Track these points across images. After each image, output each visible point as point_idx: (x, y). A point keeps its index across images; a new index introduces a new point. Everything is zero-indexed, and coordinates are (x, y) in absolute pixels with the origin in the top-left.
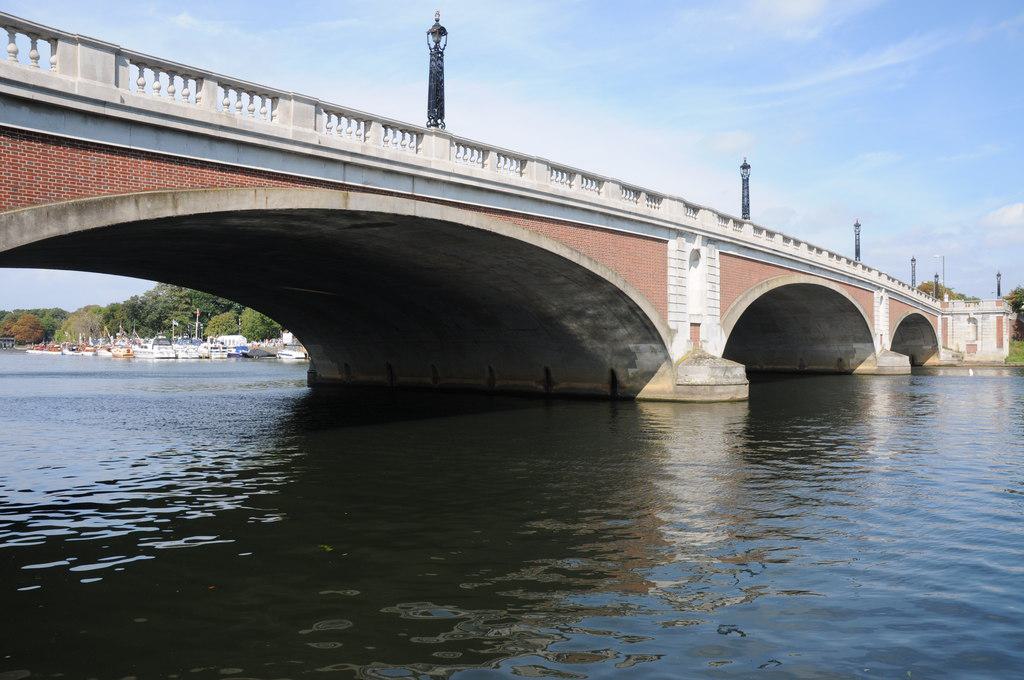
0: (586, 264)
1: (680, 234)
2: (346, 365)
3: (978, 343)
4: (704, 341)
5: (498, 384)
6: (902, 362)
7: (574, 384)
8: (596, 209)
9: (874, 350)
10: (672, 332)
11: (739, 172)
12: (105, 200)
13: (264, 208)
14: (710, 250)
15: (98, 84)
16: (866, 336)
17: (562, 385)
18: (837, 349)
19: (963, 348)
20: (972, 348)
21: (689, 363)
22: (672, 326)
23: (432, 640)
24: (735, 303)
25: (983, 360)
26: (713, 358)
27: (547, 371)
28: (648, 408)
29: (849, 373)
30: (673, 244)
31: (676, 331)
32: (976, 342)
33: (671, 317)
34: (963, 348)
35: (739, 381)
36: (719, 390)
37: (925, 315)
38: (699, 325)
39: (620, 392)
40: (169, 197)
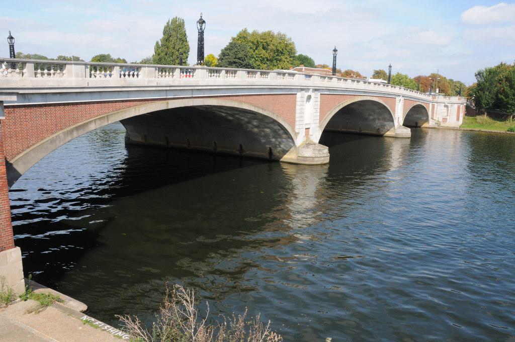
0: (261, 111)
1: (302, 90)
2: (145, 136)
3: (448, 117)
4: (311, 135)
5: (219, 150)
6: (407, 132)
7: (253, 153)
8: (266, 87)
9: (394, 125)
10: (297, 134)
11: (332, 52)
12: (85, 124)
13: (138, 114)
14: (316, 94)
15: (80, 79)
16: (391, 120)
17: (247, 153)
18: (377, 124)
19: (441, 120)
20: (445, 120)
21: (304, 147)
22: (297, 131)
23: (98, 196)
24: (326, 116)
25: (450, 126)
26: (315, 144)
27: (241, 146)
28: (285, 166)
29: (382, 136)
30: (299, 94)
31: (298, 133)
32: (447, 117)
33: (297, 127)
34: (441, 120)
35: (325, 155)
36: (316, 159)
37: (423, 104)
38: (309, 128)
39: (273, 158)
40: (106, 118)
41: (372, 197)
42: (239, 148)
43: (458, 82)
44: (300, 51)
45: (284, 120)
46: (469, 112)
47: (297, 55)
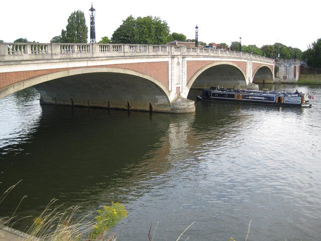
10: (170, 92)
17: (132, 108)
20: (285, 78)
41: (172, 187)
42: (127, 104)
43: (290, 47)
44: (173, 29)
45: (158, 80)
46: (302, 70)
47: (171, 33)
